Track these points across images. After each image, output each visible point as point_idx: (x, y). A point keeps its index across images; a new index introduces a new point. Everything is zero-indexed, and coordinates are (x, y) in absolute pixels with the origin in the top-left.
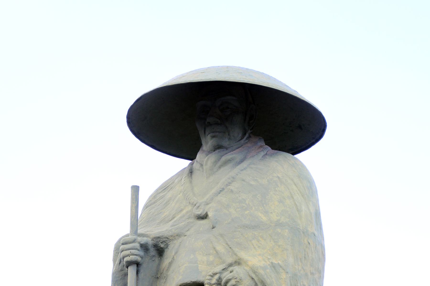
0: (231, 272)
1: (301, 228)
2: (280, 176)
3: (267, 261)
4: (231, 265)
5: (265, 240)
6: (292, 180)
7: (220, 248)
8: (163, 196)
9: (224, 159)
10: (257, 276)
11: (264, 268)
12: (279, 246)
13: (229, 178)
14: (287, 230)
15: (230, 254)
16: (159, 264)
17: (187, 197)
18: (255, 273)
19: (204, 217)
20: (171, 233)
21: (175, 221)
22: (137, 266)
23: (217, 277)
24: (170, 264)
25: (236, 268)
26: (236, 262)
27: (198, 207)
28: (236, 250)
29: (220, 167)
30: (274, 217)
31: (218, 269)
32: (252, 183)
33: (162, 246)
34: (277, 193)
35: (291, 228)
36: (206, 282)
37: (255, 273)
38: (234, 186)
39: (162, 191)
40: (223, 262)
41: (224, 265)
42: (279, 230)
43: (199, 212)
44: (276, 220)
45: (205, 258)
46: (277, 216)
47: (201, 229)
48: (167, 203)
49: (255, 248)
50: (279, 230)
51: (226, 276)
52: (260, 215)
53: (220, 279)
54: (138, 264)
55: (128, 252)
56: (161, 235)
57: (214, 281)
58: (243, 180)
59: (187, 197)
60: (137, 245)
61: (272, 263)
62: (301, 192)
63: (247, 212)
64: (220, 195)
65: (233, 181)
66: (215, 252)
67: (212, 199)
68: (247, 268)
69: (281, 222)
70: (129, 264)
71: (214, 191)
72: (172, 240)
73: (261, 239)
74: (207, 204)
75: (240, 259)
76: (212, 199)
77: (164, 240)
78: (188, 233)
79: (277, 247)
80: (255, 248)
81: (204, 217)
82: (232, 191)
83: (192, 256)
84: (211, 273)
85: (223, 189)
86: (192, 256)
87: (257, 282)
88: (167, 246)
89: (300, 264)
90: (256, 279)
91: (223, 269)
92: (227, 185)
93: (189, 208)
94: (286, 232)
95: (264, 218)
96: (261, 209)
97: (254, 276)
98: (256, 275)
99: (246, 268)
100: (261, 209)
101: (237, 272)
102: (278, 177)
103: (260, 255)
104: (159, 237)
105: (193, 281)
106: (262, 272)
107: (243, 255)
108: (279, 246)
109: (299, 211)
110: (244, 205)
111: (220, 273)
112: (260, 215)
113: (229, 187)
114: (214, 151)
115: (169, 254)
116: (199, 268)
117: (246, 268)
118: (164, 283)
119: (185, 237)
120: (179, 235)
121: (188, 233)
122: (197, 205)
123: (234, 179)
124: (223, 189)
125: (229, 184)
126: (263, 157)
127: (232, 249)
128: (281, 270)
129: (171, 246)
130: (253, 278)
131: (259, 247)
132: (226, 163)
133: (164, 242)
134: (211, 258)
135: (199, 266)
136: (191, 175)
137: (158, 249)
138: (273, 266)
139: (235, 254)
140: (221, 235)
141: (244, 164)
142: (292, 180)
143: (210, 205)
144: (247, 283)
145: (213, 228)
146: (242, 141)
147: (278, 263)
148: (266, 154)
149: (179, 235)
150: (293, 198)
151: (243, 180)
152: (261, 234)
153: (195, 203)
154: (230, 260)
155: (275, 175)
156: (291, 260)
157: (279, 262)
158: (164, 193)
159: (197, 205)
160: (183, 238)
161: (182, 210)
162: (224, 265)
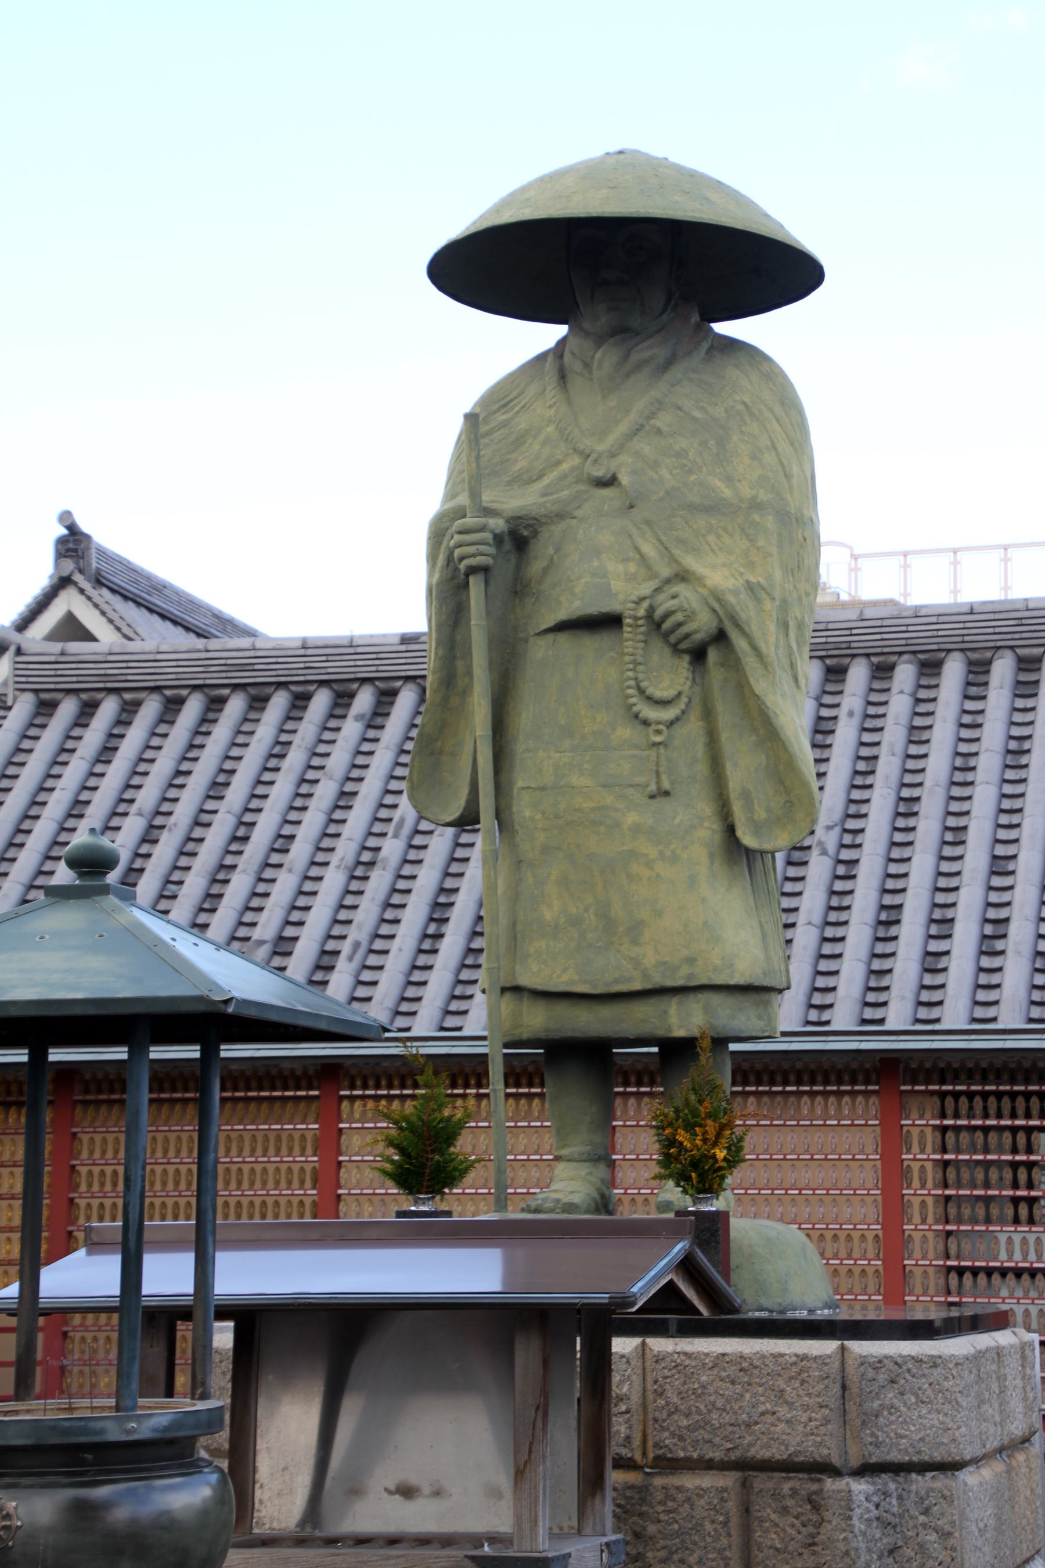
0: (674, 597)
1: (793, 511)
2: (747, 400)
3: (738, 577)
4: (668, 581)
5: (731, 535)
6: (772, 411)
7: (649, 549)
8: (504, 424)
9: (635, 357)
10: (722, 606)
11: (735, 592)
12: (758, 549)
13: (652, 404)
14: (770, 518)
15: (666, 559)
16: (518, 568)
17: (568, 435)
18: (719, 600)
19: (610, 482)
20: (543, 511)
21: (549, 485)
22: (486, 574)
23: (645, 604)
24: (546, 571)
25: (679, 588)
26: (677, 575)
27: (596, 460)
28: (678, 552)
29: (628, 375)
30: (747, 492)
31: (646, 589)
32: (697, 414)
33: (525, 533)
34: (746, 438)
35: (777, 512)
36: (627, 613)
37: (719, 600)
38: (664, 421)
39: (499, 410)
40: (654, 576)
41: (657, 581)
42: (756, 517)
43: (599, 473)
44: (749, 496)
45: (621, 568)
46: (751, 488)
47: (606, 508)
48: (519, 442)
49: (713, 550)
50: (756, 517)
51: (664, 604)
52: (718, 483)
53: (651, 610)
54: (485, 570)
55: (472, 549)
56: (524, 512)
57: (641, 612)
58: (679, 408)
59: (568, 435)
60: (488, 536)
61: (747, 582)
62: (788, 436)
63: (692, 478)
64: (636, 438)
65: (659, 409)
66: (638, 556)
67: (622, 446)
68: (704, 592)
69: (758, 500)
70: (472, 570)
71: (623, 428)
72: (547, 524)
73: (722, 533)
74: (613, 455)
75: (687, 571)
76: (622, 446)
77: (531, 522)
78: (579, 513)
79: (755, 551)
80: (713, 550)
81: (610, 482)
82: (659, 432)
83: (596, 564)
84: (634, 598)
85: (642, 426)
86: (596, 564)
87: (723, 616)
88: (535, 533)
89: (791, 579)
90: (720, 612)
91: (656, 590)
92: (649, 418)
93: (576, 460)
94: (770, 522)
95: (727, 493)
96: (718, 471)
97: (716, 606)
98: (721, 604)
99: (700, 590)
100: (718, 471)
101: (686, 598)
102: (744, 403)
103: (724, 565)
104: (520, 518)
105: (603, 611)
106: (731, 599)
107: (690, 562)
108: (758, 549)
109: (788, 476)
110: (685, 462)
111: (651, 597)
112: (718, 483)
113: (653, 422)
114: (612, 336)
115: (542, 551)
116: (612, 587)
117: (700, 590)
118: (533, 604)
119: (574, 521)
120: (560, 516)
121: (579, 513)
122: (593, 456)
123: (659, 405)
124: (642, 426)
125: (652, 416)
126: (707, 353)
127: (670, 552)
128: (764, 595)
129: (544, 534)
130: (714, 611)
131: (720, 549)
132: (639, 366)
133: (529, 526)
134: (632, 568)
135: (612, 582)
136: (565, 383)
137: (518, 538)
138: (750, 587)
139: (676, 561)
140: (648, 523)
141: (677, 372)
142: (772, 411)
143: (621, 459)
144: (705, 620)
145: (631, 507)
146: (665, 317)
147: (759, 582)
148: (712, 346)
149: (560, 516)
150: (776, 450)
151: (679, 408)
152: (722, 524)
153: (588, 451)
154: (666, 572)
155: (737, 398)
156: (778, 575)
157: (760, 579)
158: (510, 414)
159: (593, 456)
160: (568, 521)
161: (559, 463)
162: (657, 581)
